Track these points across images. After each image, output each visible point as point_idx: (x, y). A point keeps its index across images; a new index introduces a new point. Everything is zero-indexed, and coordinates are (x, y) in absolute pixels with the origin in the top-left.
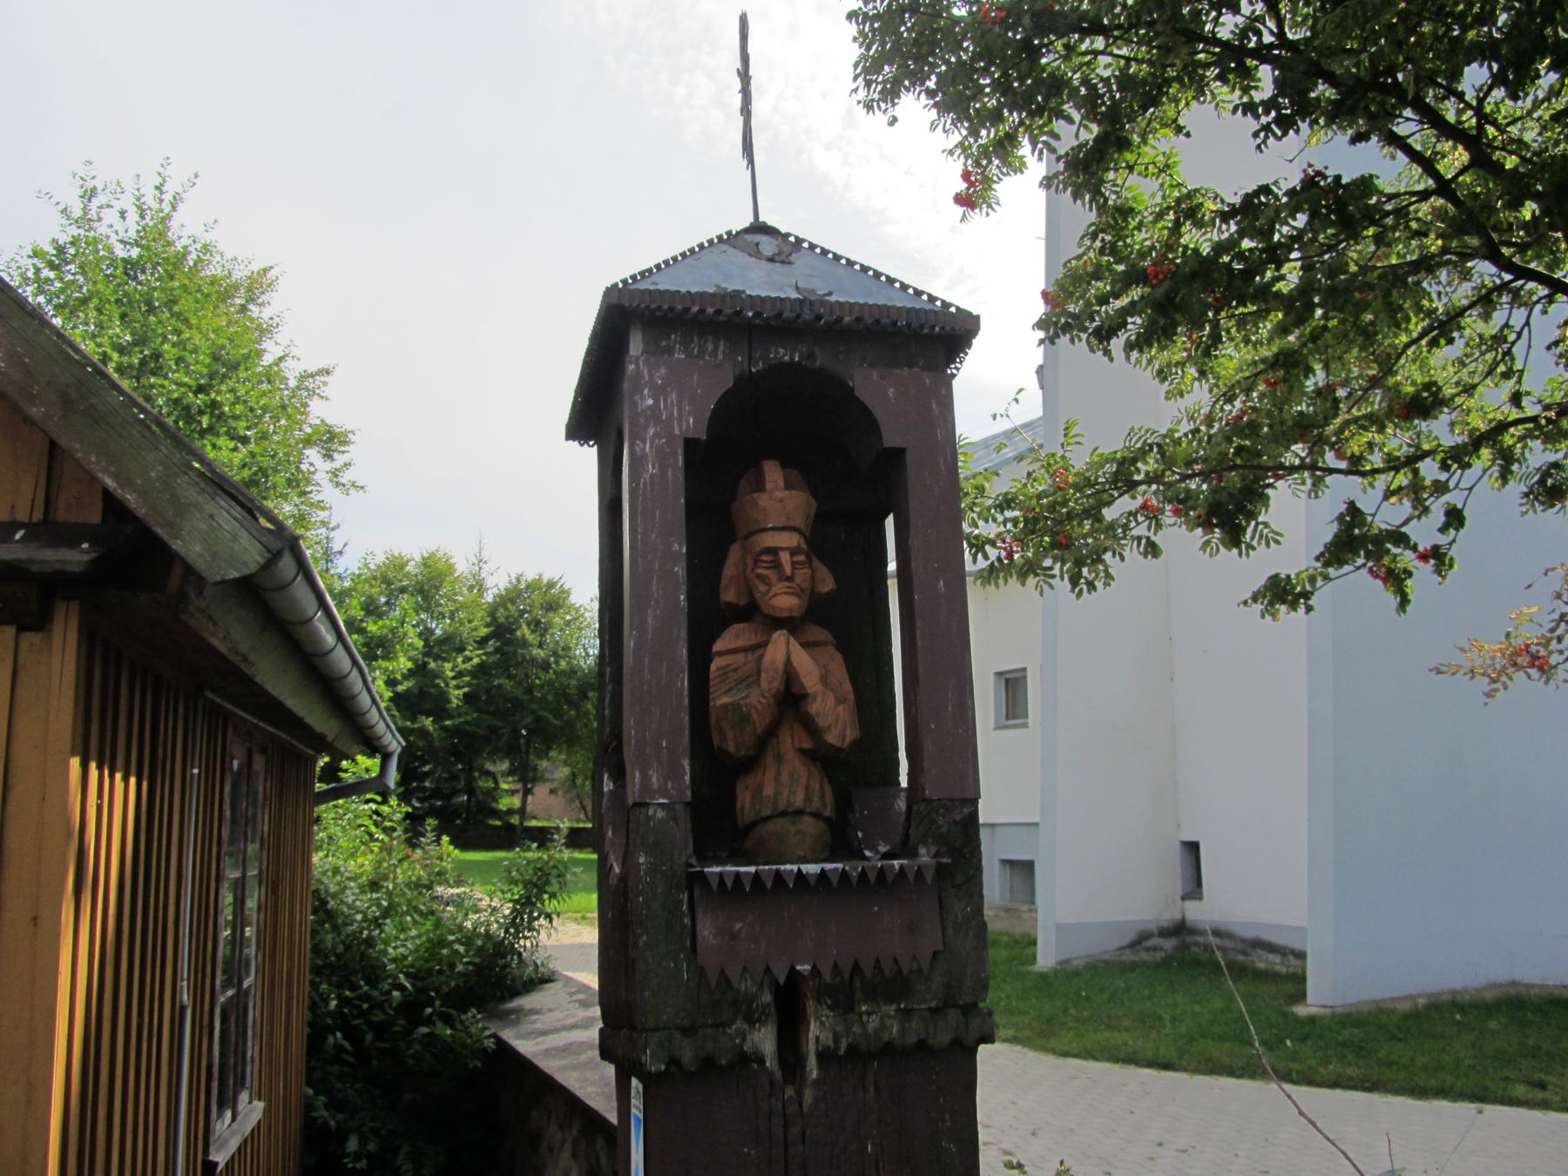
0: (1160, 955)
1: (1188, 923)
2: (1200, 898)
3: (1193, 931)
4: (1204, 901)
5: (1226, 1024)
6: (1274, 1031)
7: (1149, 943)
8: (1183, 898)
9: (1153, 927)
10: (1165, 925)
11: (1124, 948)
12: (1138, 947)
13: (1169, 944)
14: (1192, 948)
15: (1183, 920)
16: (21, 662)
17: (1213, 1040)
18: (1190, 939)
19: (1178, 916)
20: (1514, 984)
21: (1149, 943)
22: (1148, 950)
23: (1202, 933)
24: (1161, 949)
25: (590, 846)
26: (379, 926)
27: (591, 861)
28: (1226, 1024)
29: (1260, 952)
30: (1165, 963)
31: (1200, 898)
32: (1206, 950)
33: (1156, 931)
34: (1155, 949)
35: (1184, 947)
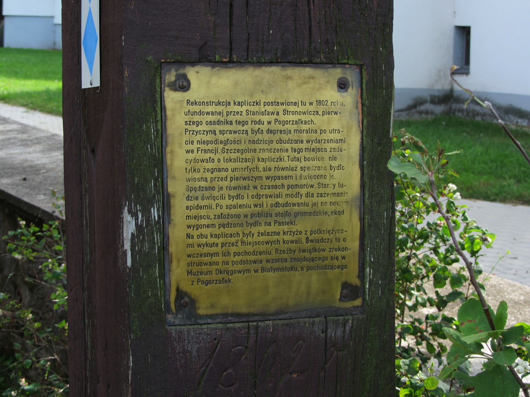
0: (430, 117)
1: (455, 94)
2: (467, 73)
3: (459, 100)
4: (470, 77)
5: (485, 163)
6: (522, 169)
7: (423, 108)
8: (453, 73)
9: (426, 95)
10: (437, 94)
11: (402, 111)
12: (414, 110)
13: (439, 109)
14: (457, 114)
15: (452, 90)
16: (523, 155)
17: (473, 173)
18: (454, 106)
19: (447, 87)
20: (511, 105)
21: (423, 108)
22: (421, 113)
23: (463, 101)
24: (432, 113)
25: (386, 166)
26: (57, 282)
27: (48, 94)
28: (485, 163)
29: (512, 117)
30: (436, 122)
31: (467, 73)
32: (468, 115)
33: (429, 98)
34: (427, 113)
35: (449, 113)
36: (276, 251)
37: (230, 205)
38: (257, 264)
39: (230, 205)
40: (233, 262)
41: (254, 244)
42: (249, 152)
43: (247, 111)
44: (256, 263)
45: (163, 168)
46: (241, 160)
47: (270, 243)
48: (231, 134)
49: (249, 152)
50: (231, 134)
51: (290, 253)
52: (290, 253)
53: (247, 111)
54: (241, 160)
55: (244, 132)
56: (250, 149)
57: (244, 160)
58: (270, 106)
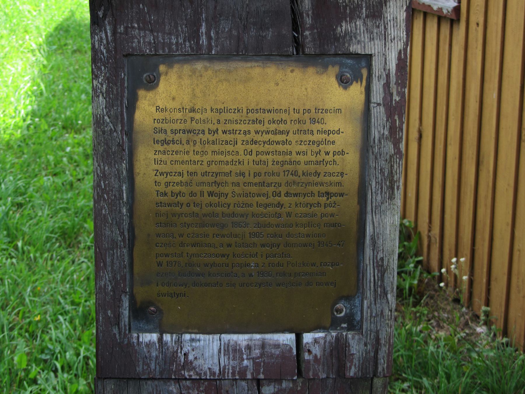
36: (157, 109)
37: (175, 130)
38: (298, 197)
39: (175, 130)
40: (279, 195)
41: (227, 153)
42: (327, 144)
43: (156, 129)
44: (297, 196)
45: (364, 241)
46: (221, 142)
47: (165, 175)
48: (185, 133)
49: (327, 144)
50: (185, 133)
51: (166, 123)
52: (166, 123)
53: (156, 129)
54: (221, 142)
55: (200, 132)
56: (328, 141)
57: (224, 142)
58: (174, 129)
